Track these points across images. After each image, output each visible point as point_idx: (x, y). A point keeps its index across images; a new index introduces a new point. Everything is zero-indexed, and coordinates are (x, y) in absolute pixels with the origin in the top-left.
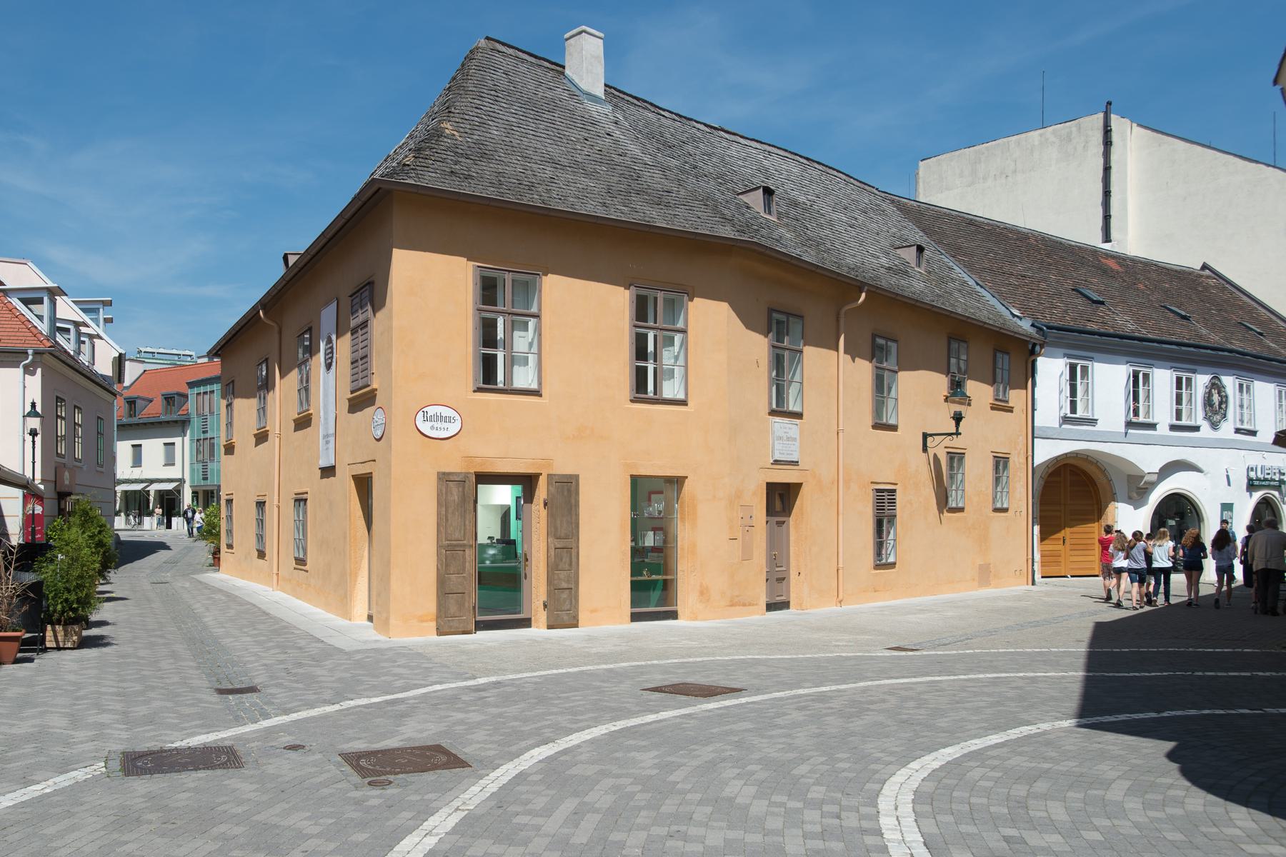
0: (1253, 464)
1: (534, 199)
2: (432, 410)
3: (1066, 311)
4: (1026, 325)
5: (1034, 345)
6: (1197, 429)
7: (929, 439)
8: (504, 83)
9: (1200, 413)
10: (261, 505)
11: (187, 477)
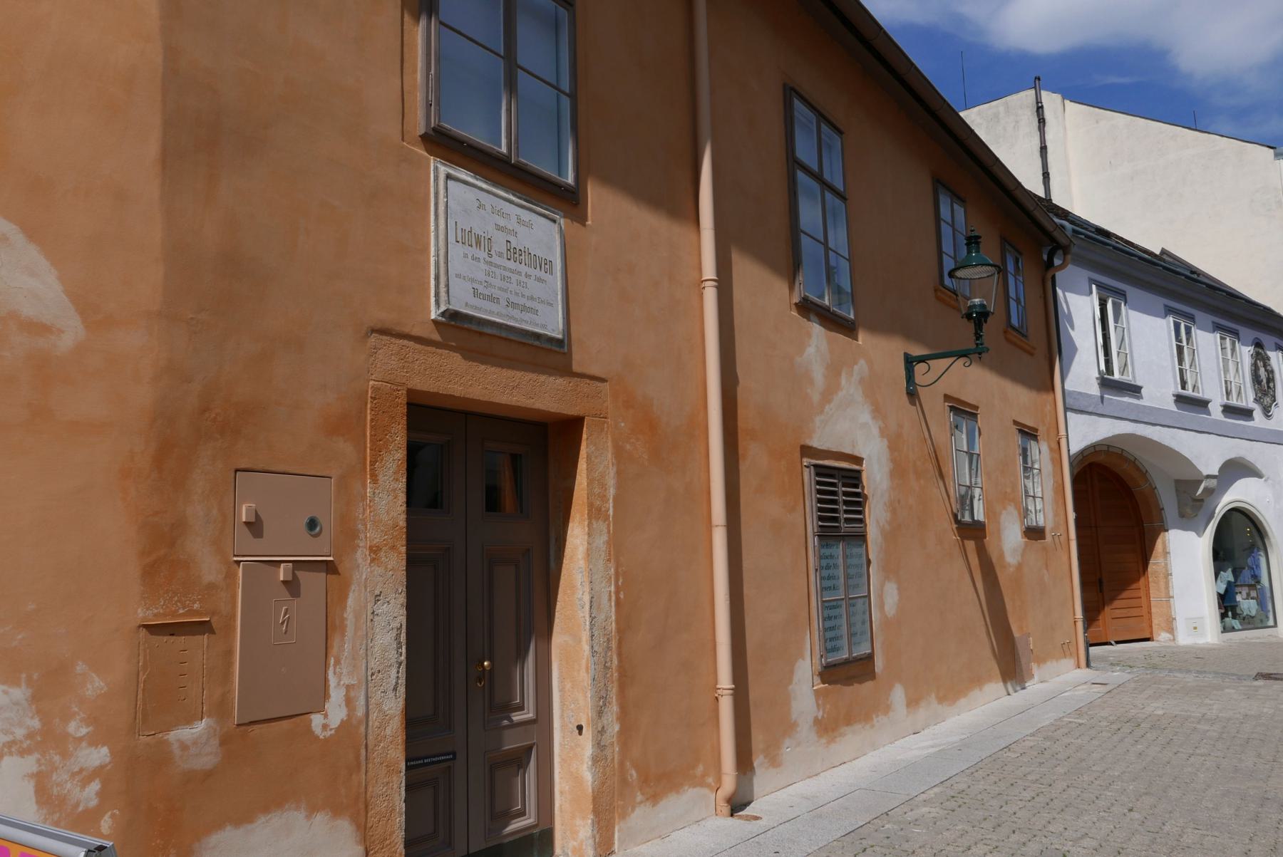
9: (1251, 395)
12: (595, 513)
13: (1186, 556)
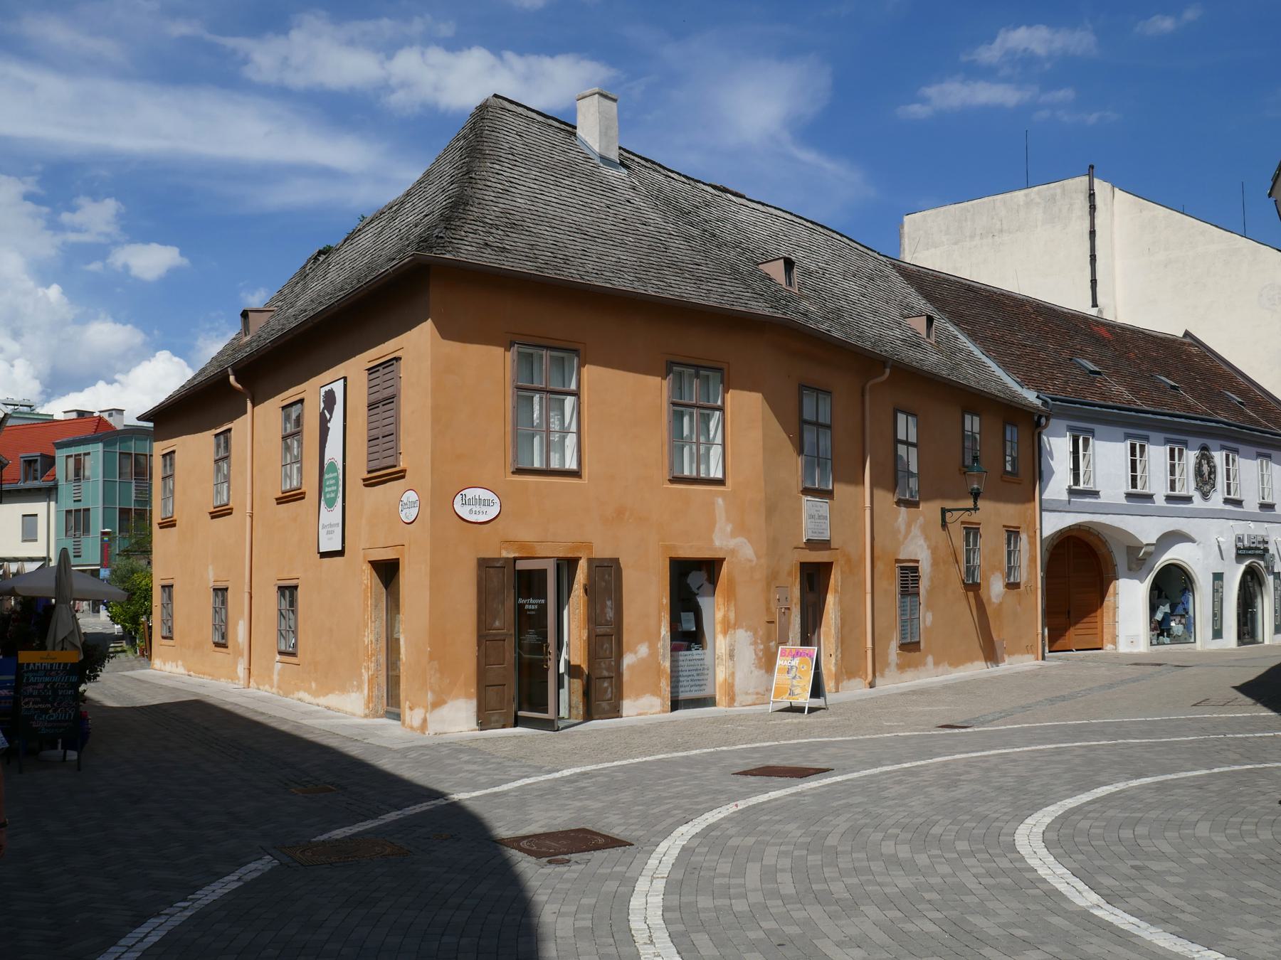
0: (1239, 532)
2: (470, 493)
3: (1066, 382)
4: (1030, 396)
5: (1040, 417)
7: (948, 515)
8: (520, 148)
9: (1193, 485)
10: (221, 592)
11: (52, 555)
12: (836, 591)
13: (1130, 599)
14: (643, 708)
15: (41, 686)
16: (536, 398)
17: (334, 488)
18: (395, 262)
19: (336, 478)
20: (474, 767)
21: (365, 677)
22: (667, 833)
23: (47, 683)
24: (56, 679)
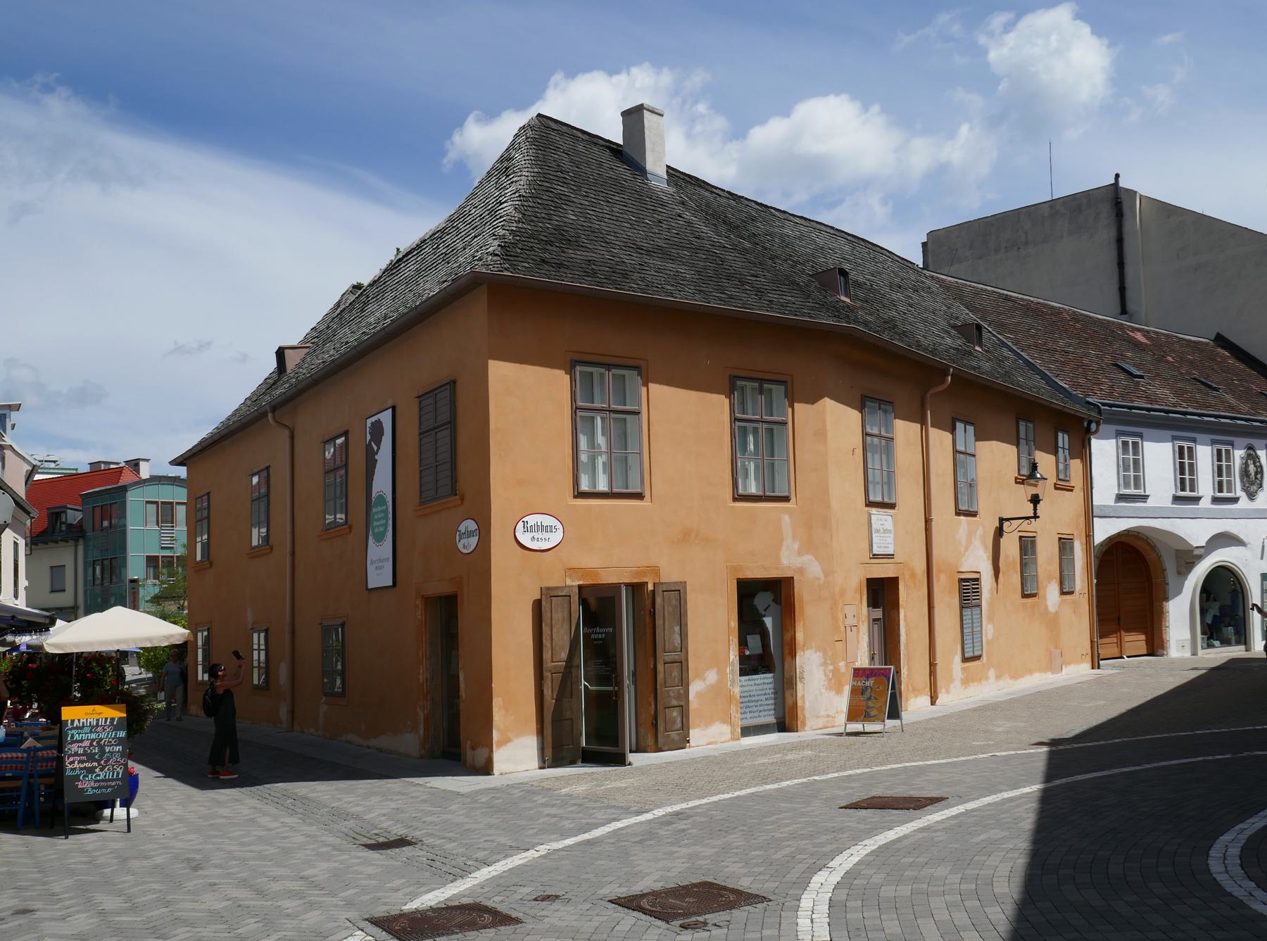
1: (633, 289)
2: (532, 520)
5: (1090, 422)
6: (1235, 500)
14: (710, 737)
15: (87, 743)
16: (599, 421)
17: (383, 522)
18: (445, 285)
19: (386, 511)
20: (553, 811)
21: (421, 716)
22: (804, 884)
23: (93, 740)
24: (102, 736)
